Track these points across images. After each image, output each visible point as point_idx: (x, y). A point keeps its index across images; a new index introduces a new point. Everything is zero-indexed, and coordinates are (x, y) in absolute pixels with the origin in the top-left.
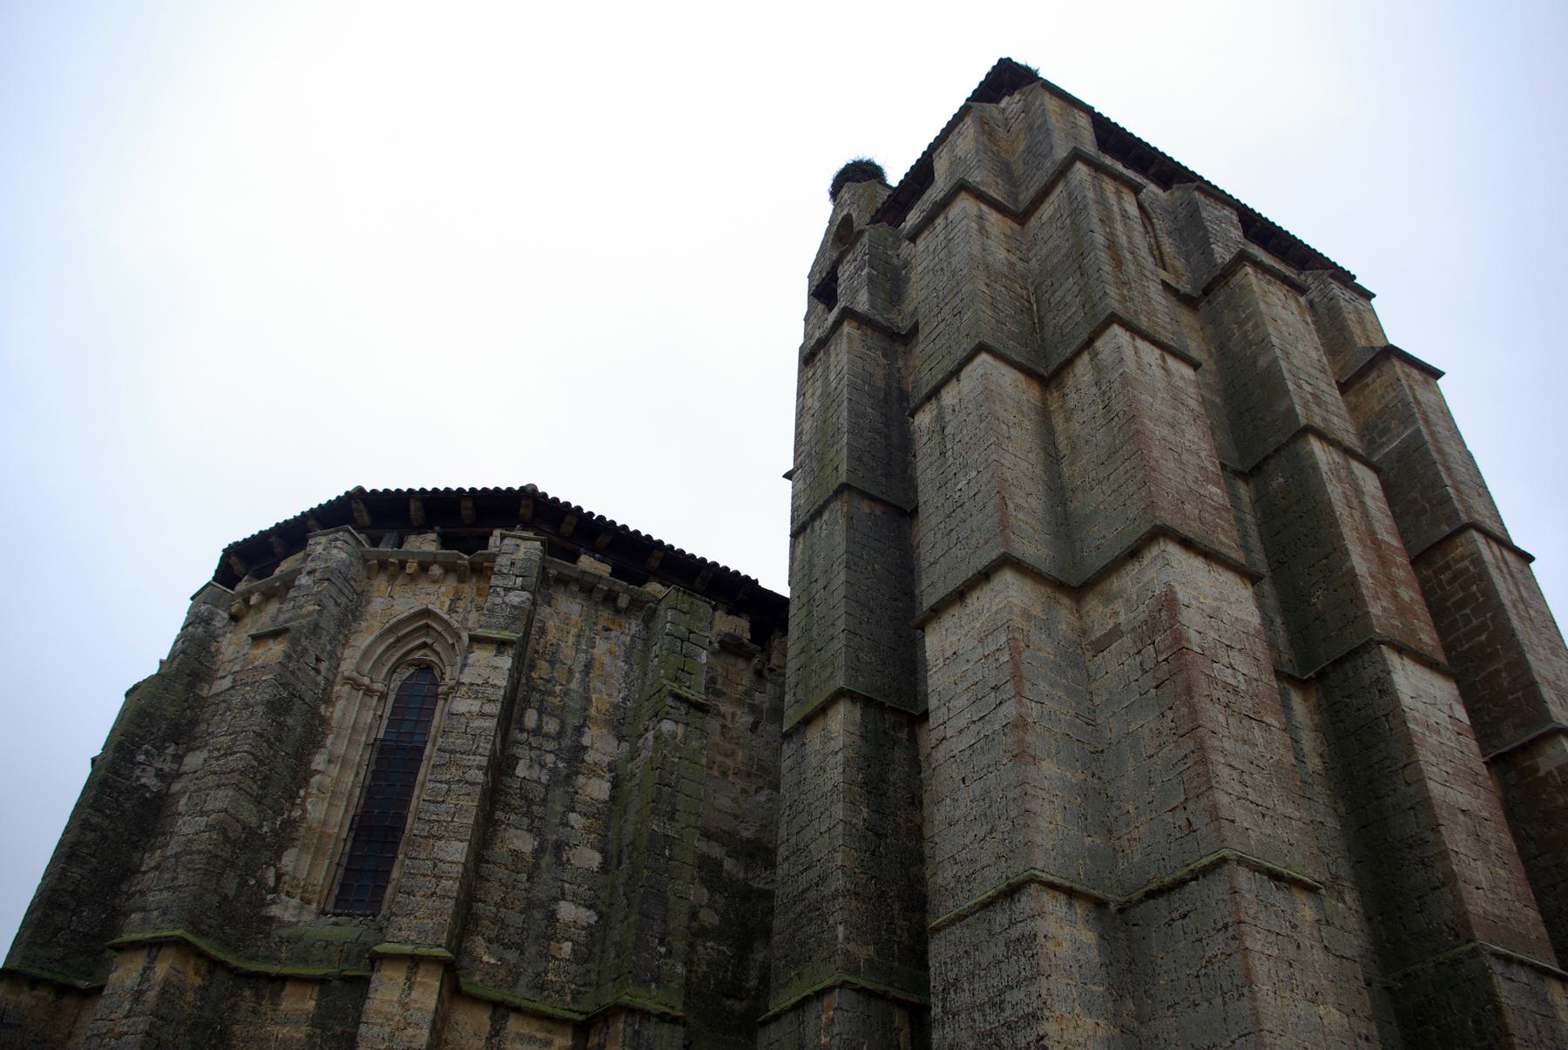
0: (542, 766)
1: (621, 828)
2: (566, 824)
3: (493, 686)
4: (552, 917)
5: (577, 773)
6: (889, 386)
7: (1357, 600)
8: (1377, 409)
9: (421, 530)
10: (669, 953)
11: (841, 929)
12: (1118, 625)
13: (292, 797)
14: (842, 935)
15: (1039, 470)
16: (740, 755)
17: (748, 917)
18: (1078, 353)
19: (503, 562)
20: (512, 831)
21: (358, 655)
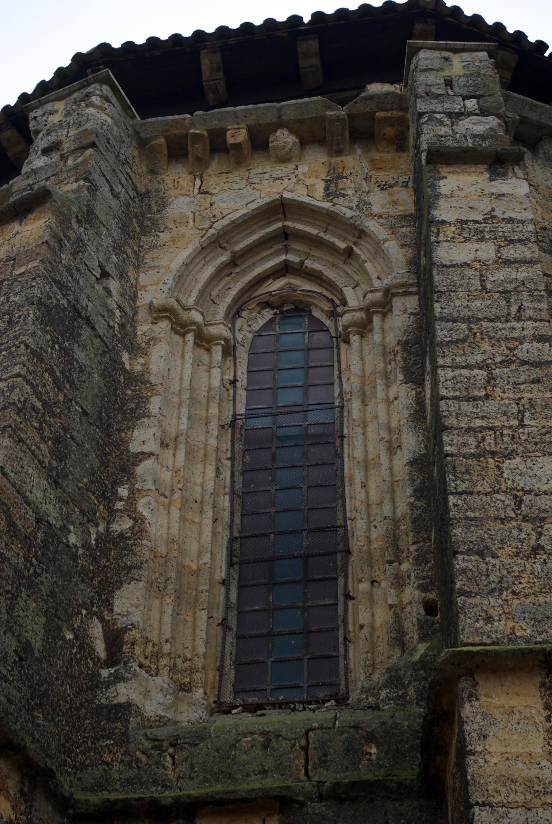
13: (108, 497)
21: (170, 279)
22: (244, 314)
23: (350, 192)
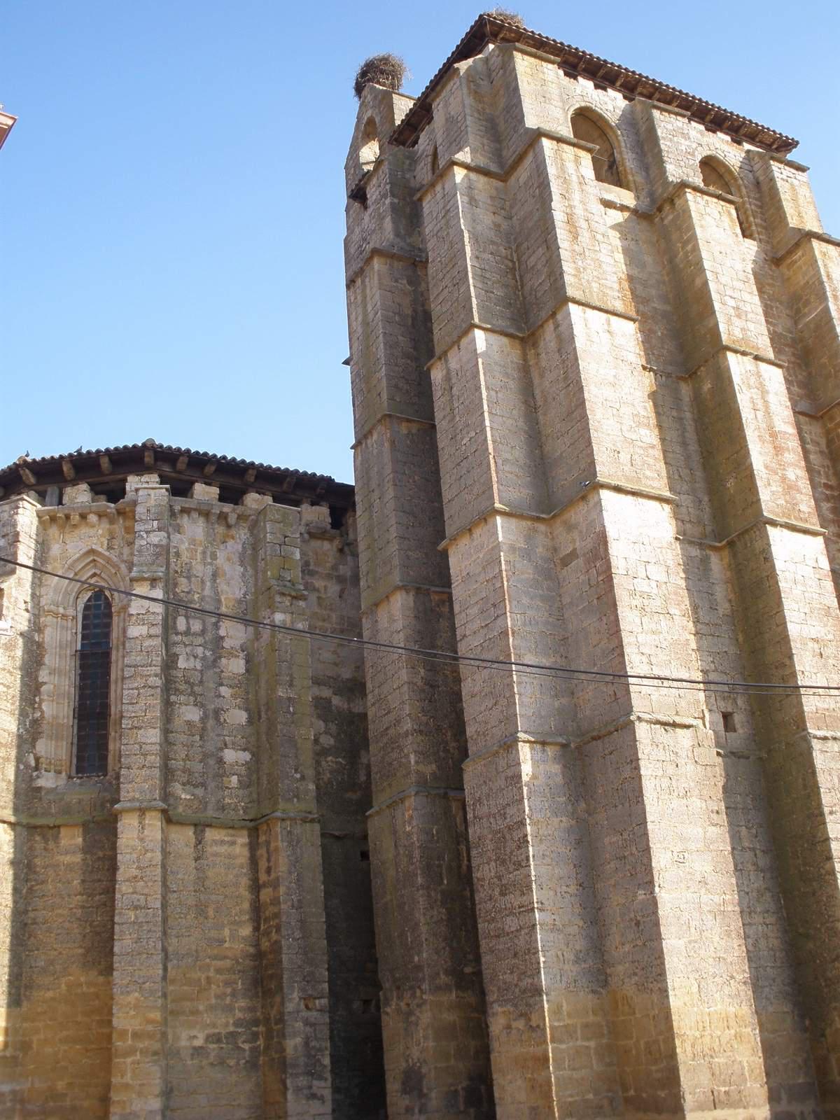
0: (195, 657)
1: (257, 691)
2: (219, 696)
3: (153, 613)
4: (221, 761)
5: (220, 658)
6: (415, 311)
7: (753, 489)
8: (802, 283)
9: (74, 482)
10: (303, 778)
11: (412, 757)
12: (575, 549)
14: (413, 759)
15: (521, 423)
16: (334, 616)
17: (352, 734)
18: (547, 321)
19: (140, 510)
20: (184, 707)
22: (80, 596)
23: (116, 547)
